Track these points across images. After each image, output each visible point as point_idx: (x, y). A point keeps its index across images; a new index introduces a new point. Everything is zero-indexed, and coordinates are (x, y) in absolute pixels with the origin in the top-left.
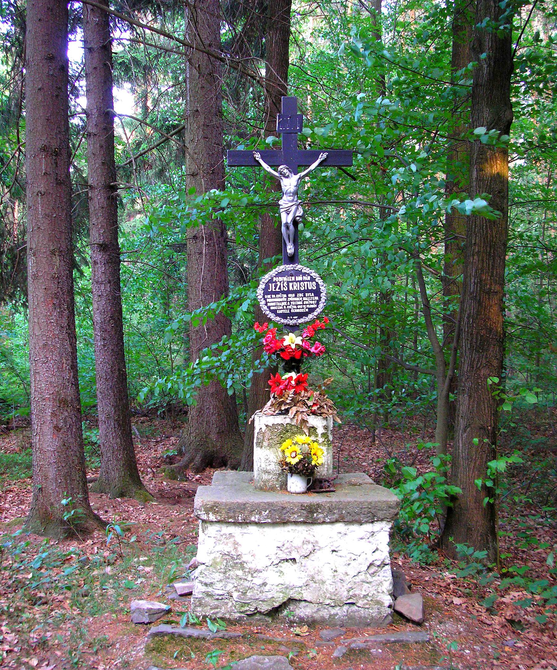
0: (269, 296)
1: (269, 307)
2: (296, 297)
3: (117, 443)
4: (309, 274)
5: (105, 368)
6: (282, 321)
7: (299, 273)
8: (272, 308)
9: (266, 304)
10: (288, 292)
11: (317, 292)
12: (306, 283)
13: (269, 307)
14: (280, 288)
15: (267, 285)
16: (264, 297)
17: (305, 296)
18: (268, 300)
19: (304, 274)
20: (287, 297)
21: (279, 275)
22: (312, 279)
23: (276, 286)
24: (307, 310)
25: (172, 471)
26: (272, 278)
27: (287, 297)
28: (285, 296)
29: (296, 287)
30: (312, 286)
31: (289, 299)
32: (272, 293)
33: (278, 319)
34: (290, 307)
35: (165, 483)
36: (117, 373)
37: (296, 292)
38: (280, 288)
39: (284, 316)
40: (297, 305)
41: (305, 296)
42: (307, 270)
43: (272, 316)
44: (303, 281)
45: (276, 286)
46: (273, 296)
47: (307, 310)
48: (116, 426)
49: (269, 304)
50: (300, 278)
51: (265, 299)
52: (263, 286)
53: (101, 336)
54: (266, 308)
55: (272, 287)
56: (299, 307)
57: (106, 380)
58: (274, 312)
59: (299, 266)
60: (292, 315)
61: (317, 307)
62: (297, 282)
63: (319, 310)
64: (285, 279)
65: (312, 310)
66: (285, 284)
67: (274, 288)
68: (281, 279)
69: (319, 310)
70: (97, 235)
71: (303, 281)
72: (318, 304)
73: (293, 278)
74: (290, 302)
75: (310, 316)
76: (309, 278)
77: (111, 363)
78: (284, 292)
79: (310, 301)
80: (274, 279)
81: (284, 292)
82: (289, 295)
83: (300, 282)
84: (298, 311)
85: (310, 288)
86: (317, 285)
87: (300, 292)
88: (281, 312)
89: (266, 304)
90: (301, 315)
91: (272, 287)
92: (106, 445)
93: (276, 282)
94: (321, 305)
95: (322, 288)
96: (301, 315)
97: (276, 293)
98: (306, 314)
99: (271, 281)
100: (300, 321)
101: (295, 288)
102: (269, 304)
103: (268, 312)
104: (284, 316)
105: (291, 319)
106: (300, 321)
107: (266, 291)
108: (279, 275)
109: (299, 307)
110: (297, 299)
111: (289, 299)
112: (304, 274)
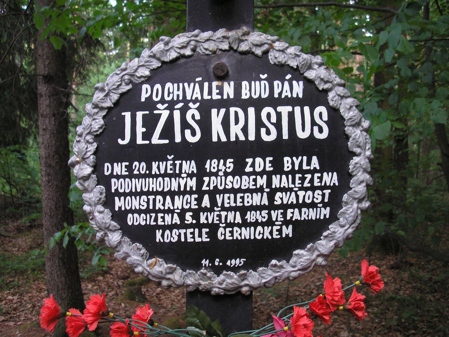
0: (119, 168)
1: (120, 216)
2: (239, 171)
3: (62, 282)
4: (297, 74)
5: (50, 205)
6: (178, 276)
7: (255, 65)
8: (130, 220)
9: (108, 202)
10: (204, 151)
11: (333, 152)
12: (285, 110)
13: (120, 216)
14: (168, 131)
15: (113, 118)
16: (97, 168)
17: (278, 169)
18: (115, 184)
19: (279, 71)
20: (201, 173)
21: (167, 70)
22: (314, 96)
23: (150, 122)
24: (288, 231)
25: (131, 292)
26: (136, 89)
27: (201, 173)
28: (189, 166)
29: (240, 127)
30: (311, 124)
31: (210, 183)
32: (133, 153)
33: (159, 267)
34: (212, 218)
35: (123, 305)
36: (62, 210)
37: (239, 152)
38: (168, 131)
39: (185, 255)
40: (243, 210)
41: (278, 169)
42: (286, 53)
43: (134, 254)
44: (273, 102)
45: (150, 122)
46: (140, 167)
47: (288, 231)
48: (61, 264)
49: (119, 203)
50: (258, 89)
51: (105, 181)
52: (98, 123)
53: (46, 171)
54: (102, 216)
55: (133, 127)
56: (251, 217)
57: (51, 217)
58: (142, 235)
59: (256, 37)
60: (218, 251)
61: (333, 218)
62: (245, 105)
63: (339, 231)
64: (192, 91)
65: (308, 232)
66: (193, 112)
67: (140, 130)
68: (172, 90)
69: (339, 231)
70: (42, 66)
71: (273, 102)
72: (335, 202)
73: (229, 90)
74: (213, 193)
75: (302, 256)
76: (298, 89)
77: (55, 199)
78: (184, 151)
79: (302, 190)
80: (145, 92)
81: (184, 151)
82: (212, 165)
83: (259, 104)
84: (246, 233)
85: (302, 135)
86: (335, 119)
87: (259, 148)
88: (172, 237)
89: (108, 202)
90: (258, 253)
91: (133, 127)
92: (51, 282)
93: (150, 104)
94: (351, 209)
95: (356, 135)
96: (258, 253)
97: (151, 154)
98: (281, 249)
99: (129, 100)
100: (256, 278)
101: (236, 130)
102: (119, 203)
103: (114, 238)
104: (185, 255)
105: (218, 271)
106: (256, 278)
107: (108, 147)
108: (167, 70)
109: (251, 217)
110: (246, 182)
111: (210, 183)
112: (279, 71)
